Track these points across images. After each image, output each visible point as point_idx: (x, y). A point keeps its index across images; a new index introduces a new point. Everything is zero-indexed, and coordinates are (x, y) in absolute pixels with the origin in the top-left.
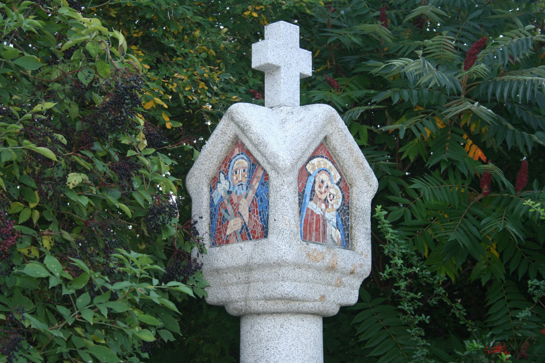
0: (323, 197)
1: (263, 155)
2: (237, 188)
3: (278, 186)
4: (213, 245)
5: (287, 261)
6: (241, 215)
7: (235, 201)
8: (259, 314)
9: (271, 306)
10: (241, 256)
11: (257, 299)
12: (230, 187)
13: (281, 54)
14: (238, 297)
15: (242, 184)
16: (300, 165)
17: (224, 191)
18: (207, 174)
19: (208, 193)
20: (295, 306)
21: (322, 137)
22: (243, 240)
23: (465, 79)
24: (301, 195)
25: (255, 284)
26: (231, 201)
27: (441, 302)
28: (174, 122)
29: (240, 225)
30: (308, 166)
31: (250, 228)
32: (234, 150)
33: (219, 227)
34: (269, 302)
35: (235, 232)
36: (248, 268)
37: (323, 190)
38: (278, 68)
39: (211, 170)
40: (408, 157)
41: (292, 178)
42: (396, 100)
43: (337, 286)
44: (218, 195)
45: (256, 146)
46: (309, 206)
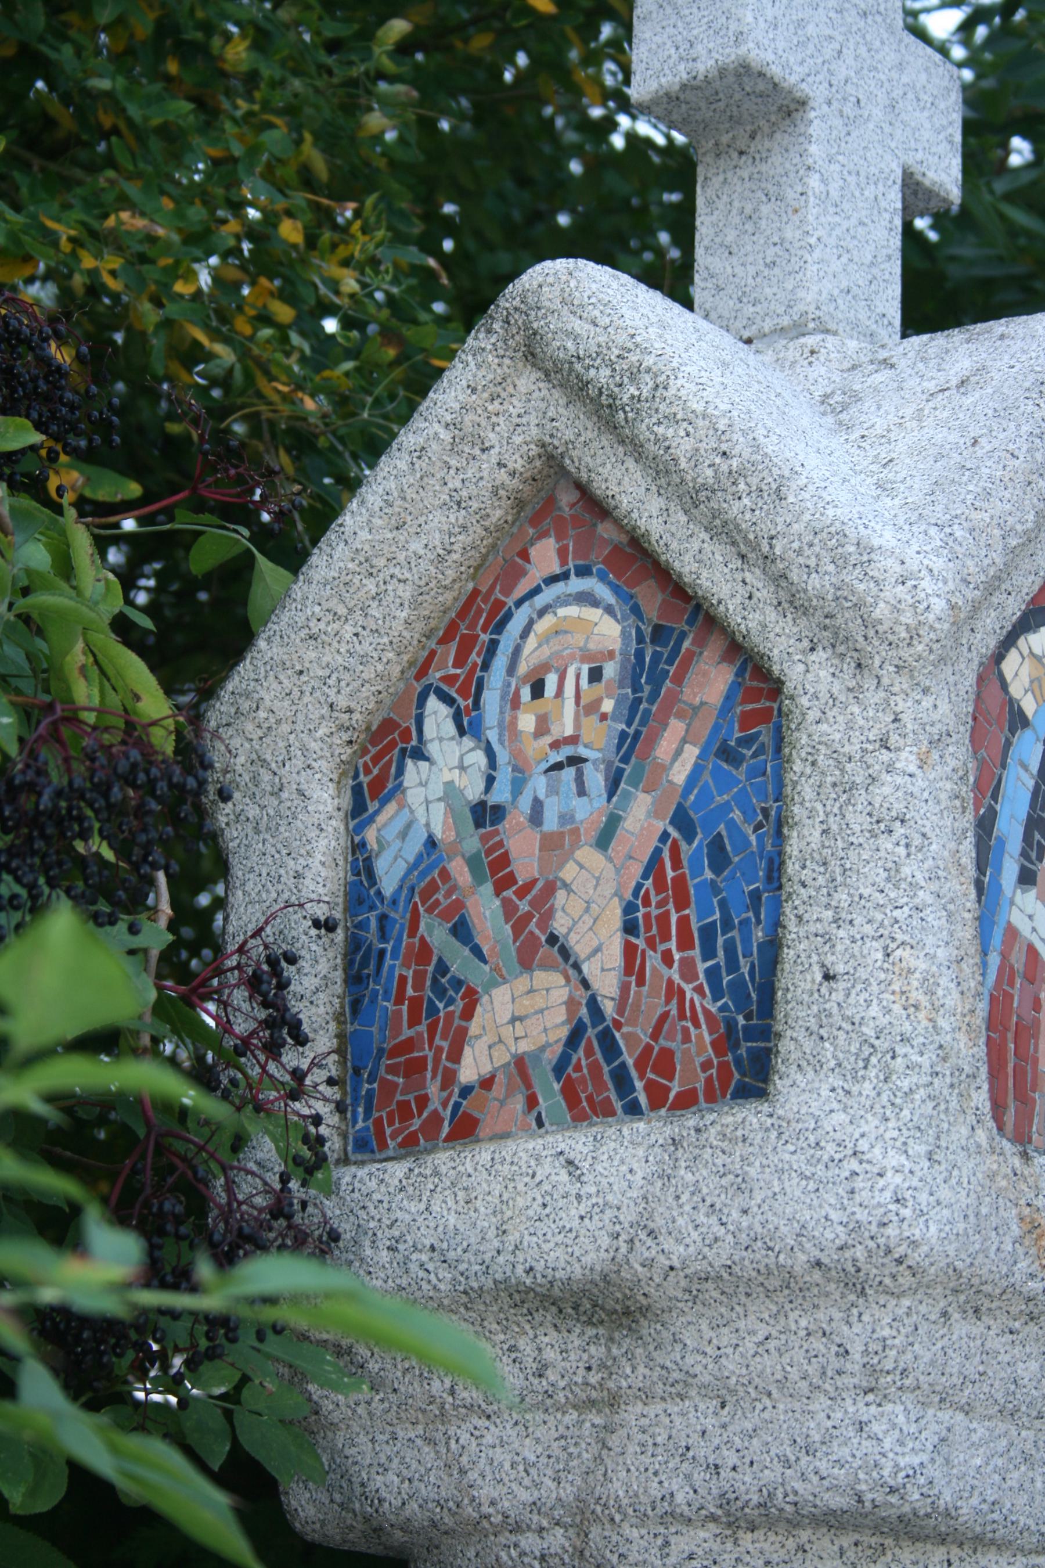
2: (539, 784)
3: (853, 748)
5: (915, 1258)
6: (565, 953)
10: (570, 1217)
11: (671, 1516)
12: (490, 781)
13: (811, 29)
14: (524, 1496)
15: (575, 761)
17: (450, 809)
18: (342, 702)
19: (337, 824)
22: (579, 1117)
25: (652, 1410)
28: (92, 470)
29: (560, 1015)
30: (1011, 664)
32: (525, 555)
33: (407, 1033)
34: (746, 1539)
35: (520, 1063)
39: (369, 674)
41: (944, 707)
44: (403, 835)
46: (1017, 919)
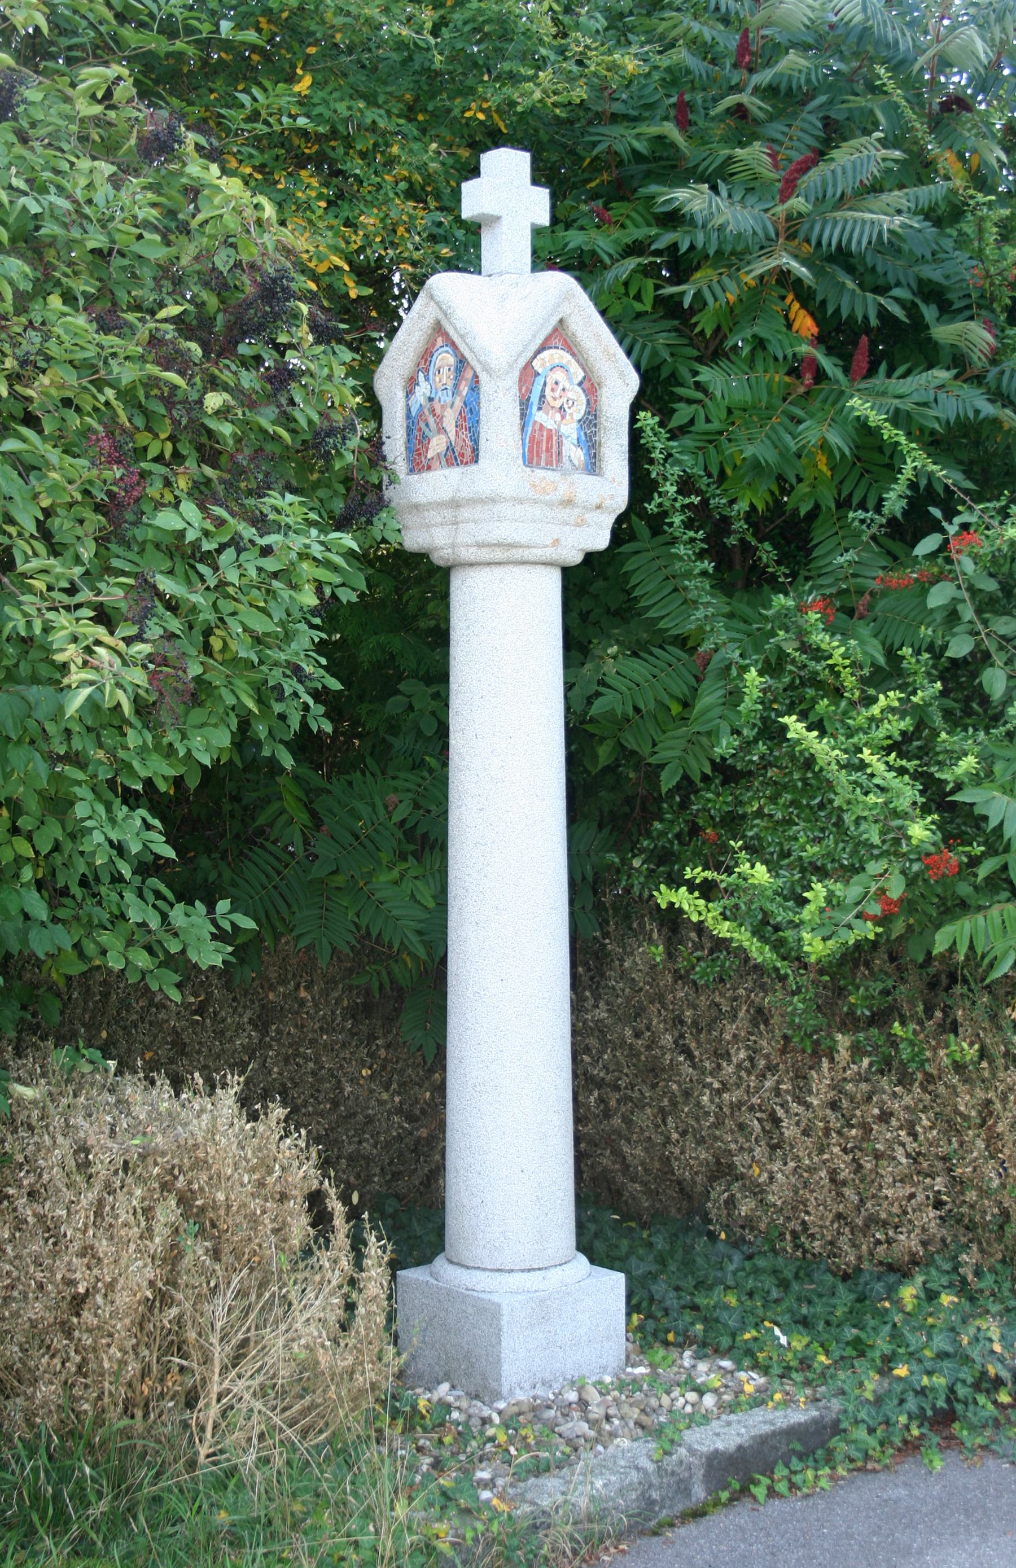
0: (558, 404)
1: (471, 350)
4: (412, 471)
7: (438, 412)
8: (472, 565)
9: (485, 555)
16: (522, 362)
20: (517, 554)
21: (554, 321)
23: (783, 217)
24: (525, 404)
26: (433, 411)
27: (742, 540)
31: (457, 449)
36: (455, 504)
37: (557, 394)
38: (498, 218)
40: (702, 331)
42: (684, 247)
43: (577, 525)
45: (462, 337)
